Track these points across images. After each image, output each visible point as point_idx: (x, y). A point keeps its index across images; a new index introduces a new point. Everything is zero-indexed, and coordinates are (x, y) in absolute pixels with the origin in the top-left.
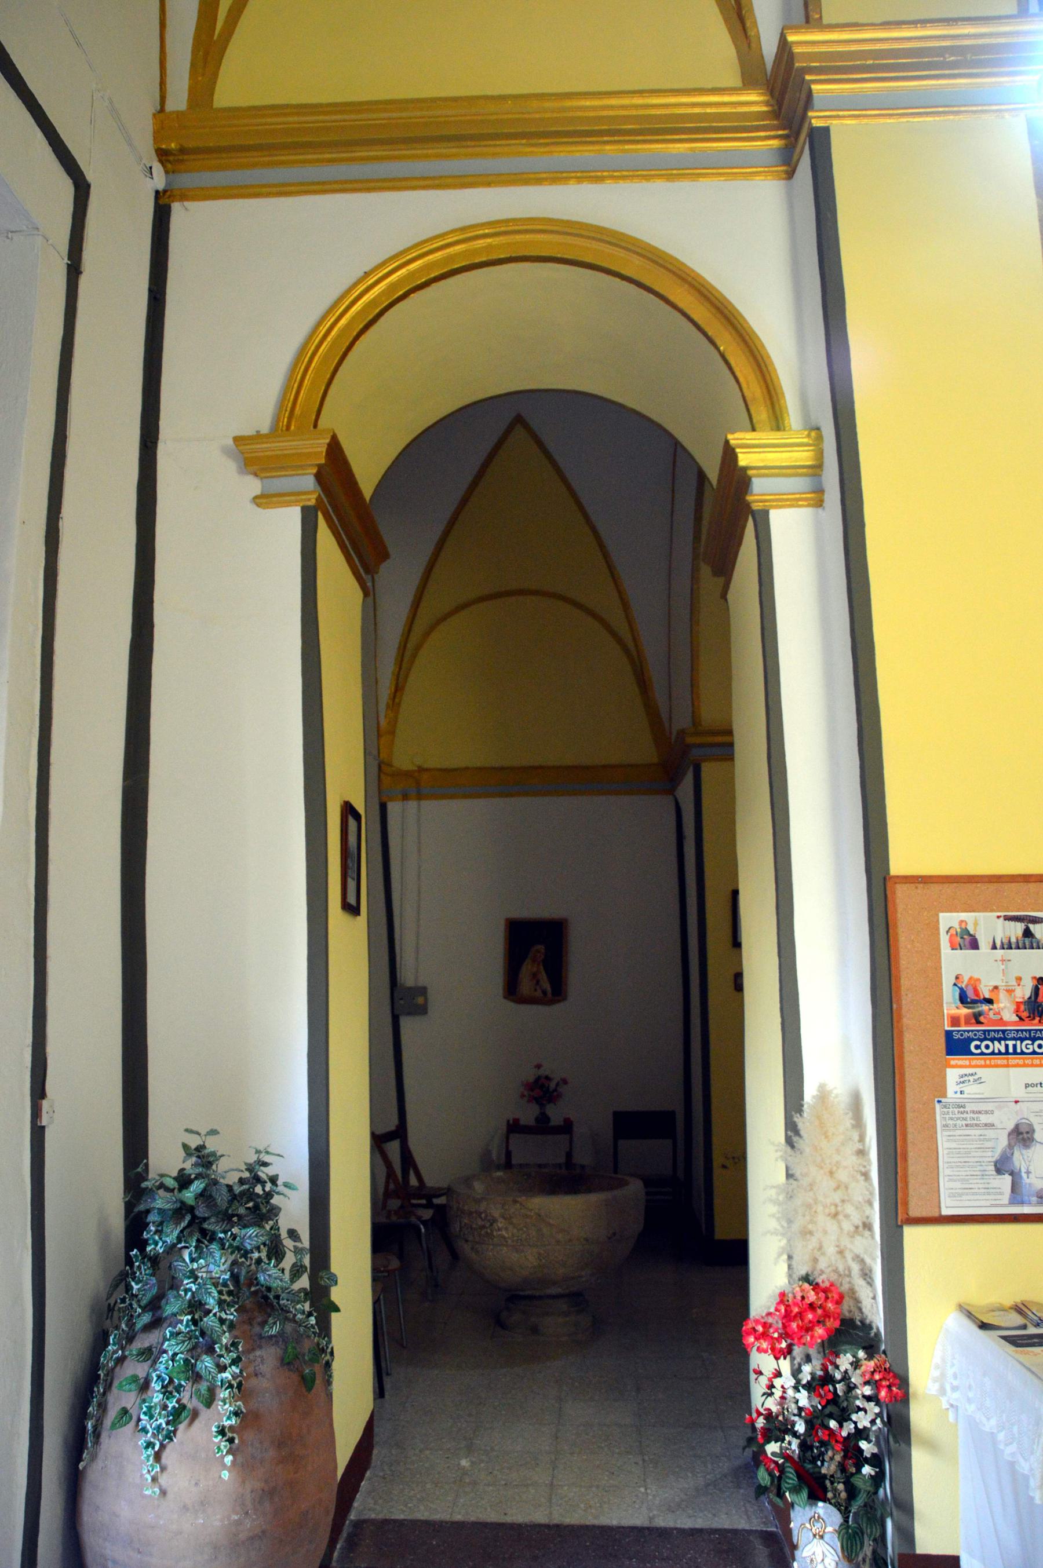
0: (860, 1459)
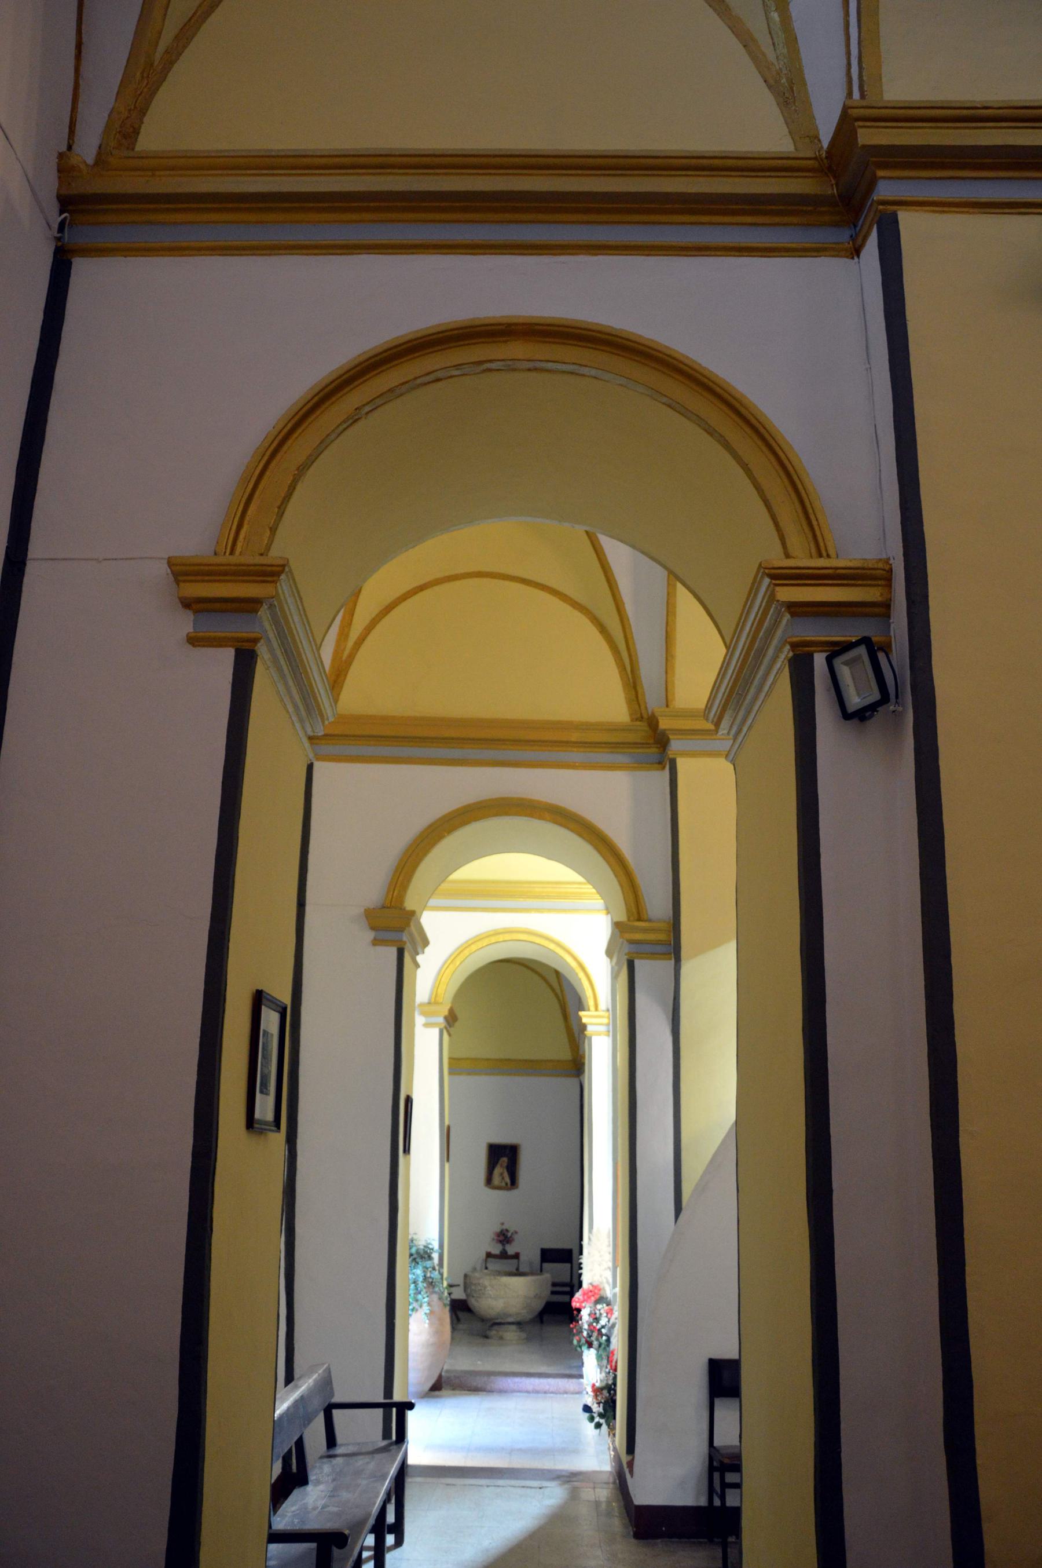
0: (601, 1335)
